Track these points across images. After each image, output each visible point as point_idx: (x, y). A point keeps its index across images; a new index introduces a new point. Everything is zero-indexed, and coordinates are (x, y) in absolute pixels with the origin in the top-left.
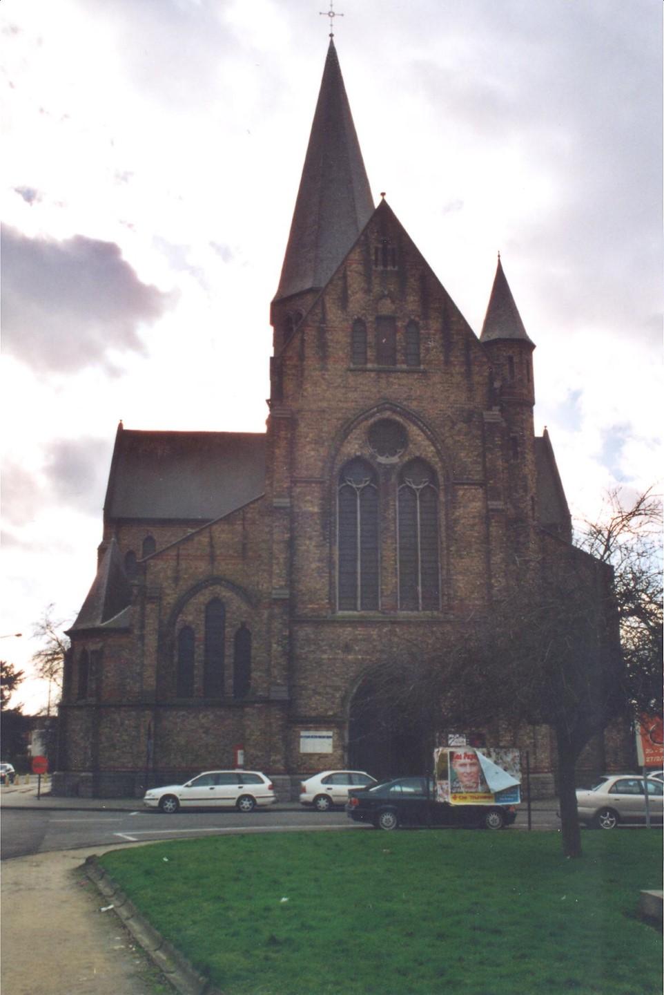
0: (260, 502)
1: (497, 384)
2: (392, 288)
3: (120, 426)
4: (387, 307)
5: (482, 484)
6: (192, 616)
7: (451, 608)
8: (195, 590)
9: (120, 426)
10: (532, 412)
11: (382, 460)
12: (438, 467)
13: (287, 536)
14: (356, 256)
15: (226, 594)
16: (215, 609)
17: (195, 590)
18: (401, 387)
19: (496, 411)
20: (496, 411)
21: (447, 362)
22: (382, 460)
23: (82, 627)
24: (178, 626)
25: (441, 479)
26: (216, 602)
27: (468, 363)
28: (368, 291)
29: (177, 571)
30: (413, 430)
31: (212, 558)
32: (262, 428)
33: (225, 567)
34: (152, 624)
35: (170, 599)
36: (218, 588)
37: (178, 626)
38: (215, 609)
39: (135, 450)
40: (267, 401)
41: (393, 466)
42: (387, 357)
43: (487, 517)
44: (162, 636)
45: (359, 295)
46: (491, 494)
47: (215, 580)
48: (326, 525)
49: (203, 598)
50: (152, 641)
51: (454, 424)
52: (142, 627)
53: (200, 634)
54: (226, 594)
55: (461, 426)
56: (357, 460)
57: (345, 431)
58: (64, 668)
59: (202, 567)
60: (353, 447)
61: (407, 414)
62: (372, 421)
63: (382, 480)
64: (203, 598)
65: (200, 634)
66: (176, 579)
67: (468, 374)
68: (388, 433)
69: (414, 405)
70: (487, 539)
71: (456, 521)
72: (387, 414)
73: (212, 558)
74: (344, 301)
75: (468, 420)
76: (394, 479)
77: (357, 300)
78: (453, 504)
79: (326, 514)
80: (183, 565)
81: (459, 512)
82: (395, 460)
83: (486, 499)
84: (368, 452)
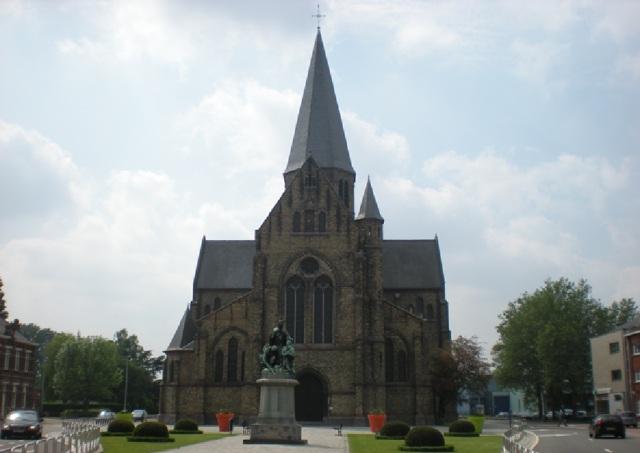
0: (246, 359)
1: (363, 239)
2: (313, 197)
3: (204, 238)
5: (353, 286)
6: (223, 345)
7: (338, 342)
8: (226, 331)
9: (204, 238)
10: (285, 181)
11: (306, 276)
12: (333, 280)
13: (261, 311)
15: (238, 335)
16: (233, 343)
17: (226, 331)
19: (361, 253)
20: (361, 253)
21: (338, 231)
22: (306, 276)
23: (171, 349)
24: (216, 349)
25: (334, 284)
27: (348, 231)
30: (323, 264)
31: (232, 319)
32: (253, 239)
33: (240, 323)
34: (203, 348)
35: (212, 337)
37: (216, 349)
38: (233, 343)
39: (207, 247)
41: (312, 279)
42: (309, 228)
43: (355, 302)
44: (208, 354)
46: (358, 291)
47: (234, 328)
48: (280, 306)
49: (227, 337)
50: (203, 357)
51: (341, 259)
52: (199, 350)
53: (226, 353)
54: (238, 335)
55: (345, 260)
57: (289, 264)
59: (227, 323)
60: (294, 270)
61: (318, 255)
62: (302, 258)
63: (306, 284)
64: (227, 337)
65: (226, 353)
66: (215, 329)
67: (348, 236)
69: (322, 251)
70: (354, 312)
71: (341, 303)
72: (309, 255)
73: (232, 319)
75: (348, 257)
76: (312, 284)
78: (340, 295)
79: (280, 300)
80: (218, 322)
81: (342, 300)
82: (312, 276)
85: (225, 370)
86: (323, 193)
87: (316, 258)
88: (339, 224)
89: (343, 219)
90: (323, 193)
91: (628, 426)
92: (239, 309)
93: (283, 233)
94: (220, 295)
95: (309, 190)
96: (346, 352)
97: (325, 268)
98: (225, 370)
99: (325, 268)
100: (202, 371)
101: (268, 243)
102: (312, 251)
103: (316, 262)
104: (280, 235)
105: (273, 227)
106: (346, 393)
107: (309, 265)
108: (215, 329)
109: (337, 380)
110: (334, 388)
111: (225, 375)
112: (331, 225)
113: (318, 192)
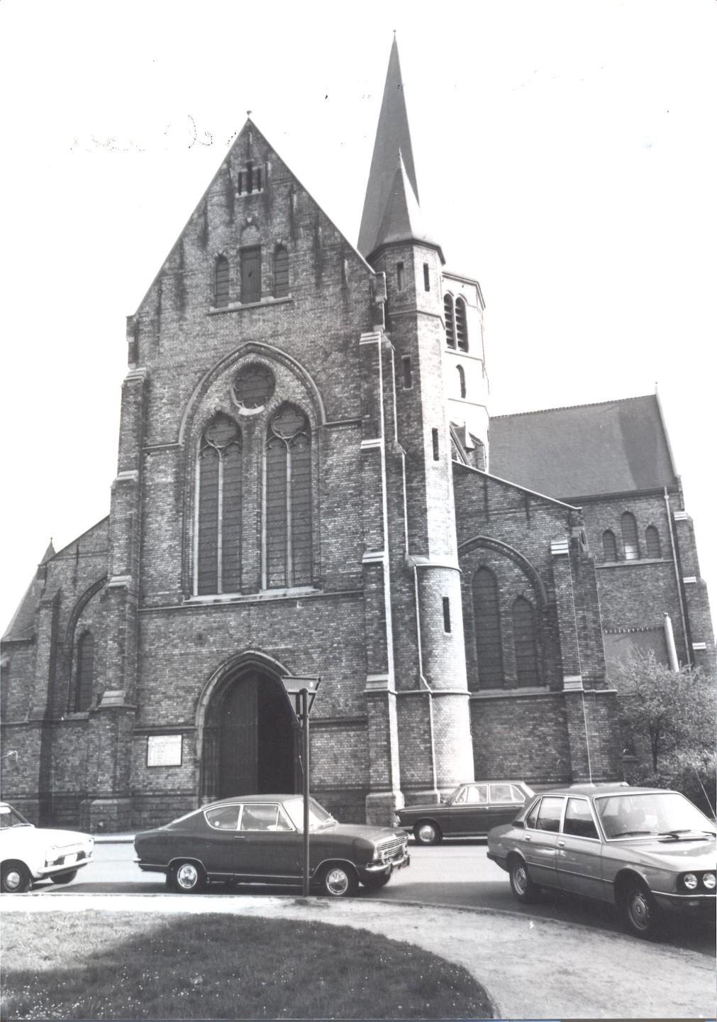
4: (251, 236)
18: (259, 326)
45: (221, 229)
68: (254, 379)
72: (251, 358)
75: (344, 348)
87: (265, 361)
91: (318, 724)
97: (289, 386)
99: (289, 386)
101: (156, 343)
102: (256, 349)
104: (182, 318)
107: (254, 379)
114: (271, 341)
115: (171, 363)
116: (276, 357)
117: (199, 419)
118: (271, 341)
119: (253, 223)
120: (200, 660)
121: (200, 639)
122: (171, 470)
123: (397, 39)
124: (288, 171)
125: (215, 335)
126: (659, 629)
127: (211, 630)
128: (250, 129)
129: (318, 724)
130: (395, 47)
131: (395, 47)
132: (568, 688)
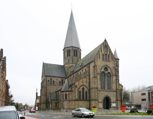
4: (106, 53)
6: (81, 90)
8: (81, 86)
14: (103, 46)
15: (84, 87)
16: (83, 89)
17: (81, 86)
18: (108, 63)
21: (112, 61)
26: (83, 88)
28: (104, 51)
29: (79, 84)
30: (109, 69)
31: (83, 82)
33: (84, 84)
34: (77, 90)
35: (78, 87)
36: (83, 86)
37: (79, 91)
38: (83, 89)
40: (46, 66)
45: (103, 51)
47: (83, 85)
49: (82, 87)
50: (77, 92)
53: (81, 92)
54: (84, 87)
56: (103, 72)
57: (102, 68)
58: (111, 103)
59: (82, 84)
60: (103, 70)
64: (82, 87)
65: (81, 92)
66: (79, 85)
68: (106, 69)
72: (106, 66)
73: (83, 82)
74: (101, 51)
75: (114, 68)
77: (103, 51)
78: (113, 78)
81: (113, 79)
83: (116, 78)
84: (104, 71)
85: (81, 96)
86: (109, 50)
87: (107, 67)
88: (112, 59)
89: (113, 58)
90: (109, 50)
91: (113, 102)
92: (84, 80)
93: (100, 60)
94: (52, 78)
95: (106, 49)
96: (114, 92)
97: (109, 71)
98: (81, 96)
99: (109, 71)
100: (77, 98)
101: (97, 62)
102: (107, 66)
103: (107, 68)
104: (99, 60)
105: (98, 58)
106: (115, 102)
107: (106, 69)
108: (79, 85)
109: (113, 99)
110: (112, 101)
111: (85, 98)
112: (110, 59)
113: (108, 50)
114: (69, 59)
115: (99, 65)
116: (109, 67)
117: (101, 72)
118: (69, 59)
119: (106, 52)
120: (102, 96)
121: (103, 94)
122: (99, 76)
123: (72, 11)
124: (68, 31)
125: (103, 63)
126: (90, 108)
127: (103, 93)
128: (105, 40)
129: (113, 102)
130: (72, 12)
131: (72, 12)
132: (115, 104)
